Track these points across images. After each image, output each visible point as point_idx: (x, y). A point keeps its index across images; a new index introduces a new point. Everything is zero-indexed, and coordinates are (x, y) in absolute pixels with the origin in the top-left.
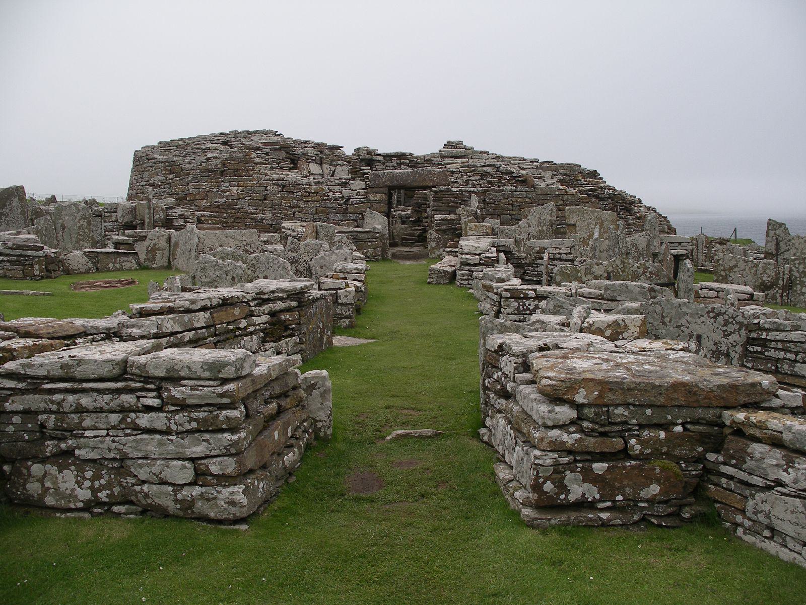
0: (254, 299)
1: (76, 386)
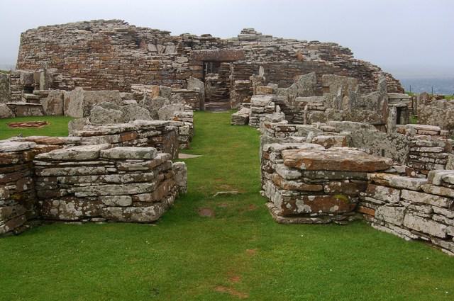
0: (140, 129)
1: (76, 163)
